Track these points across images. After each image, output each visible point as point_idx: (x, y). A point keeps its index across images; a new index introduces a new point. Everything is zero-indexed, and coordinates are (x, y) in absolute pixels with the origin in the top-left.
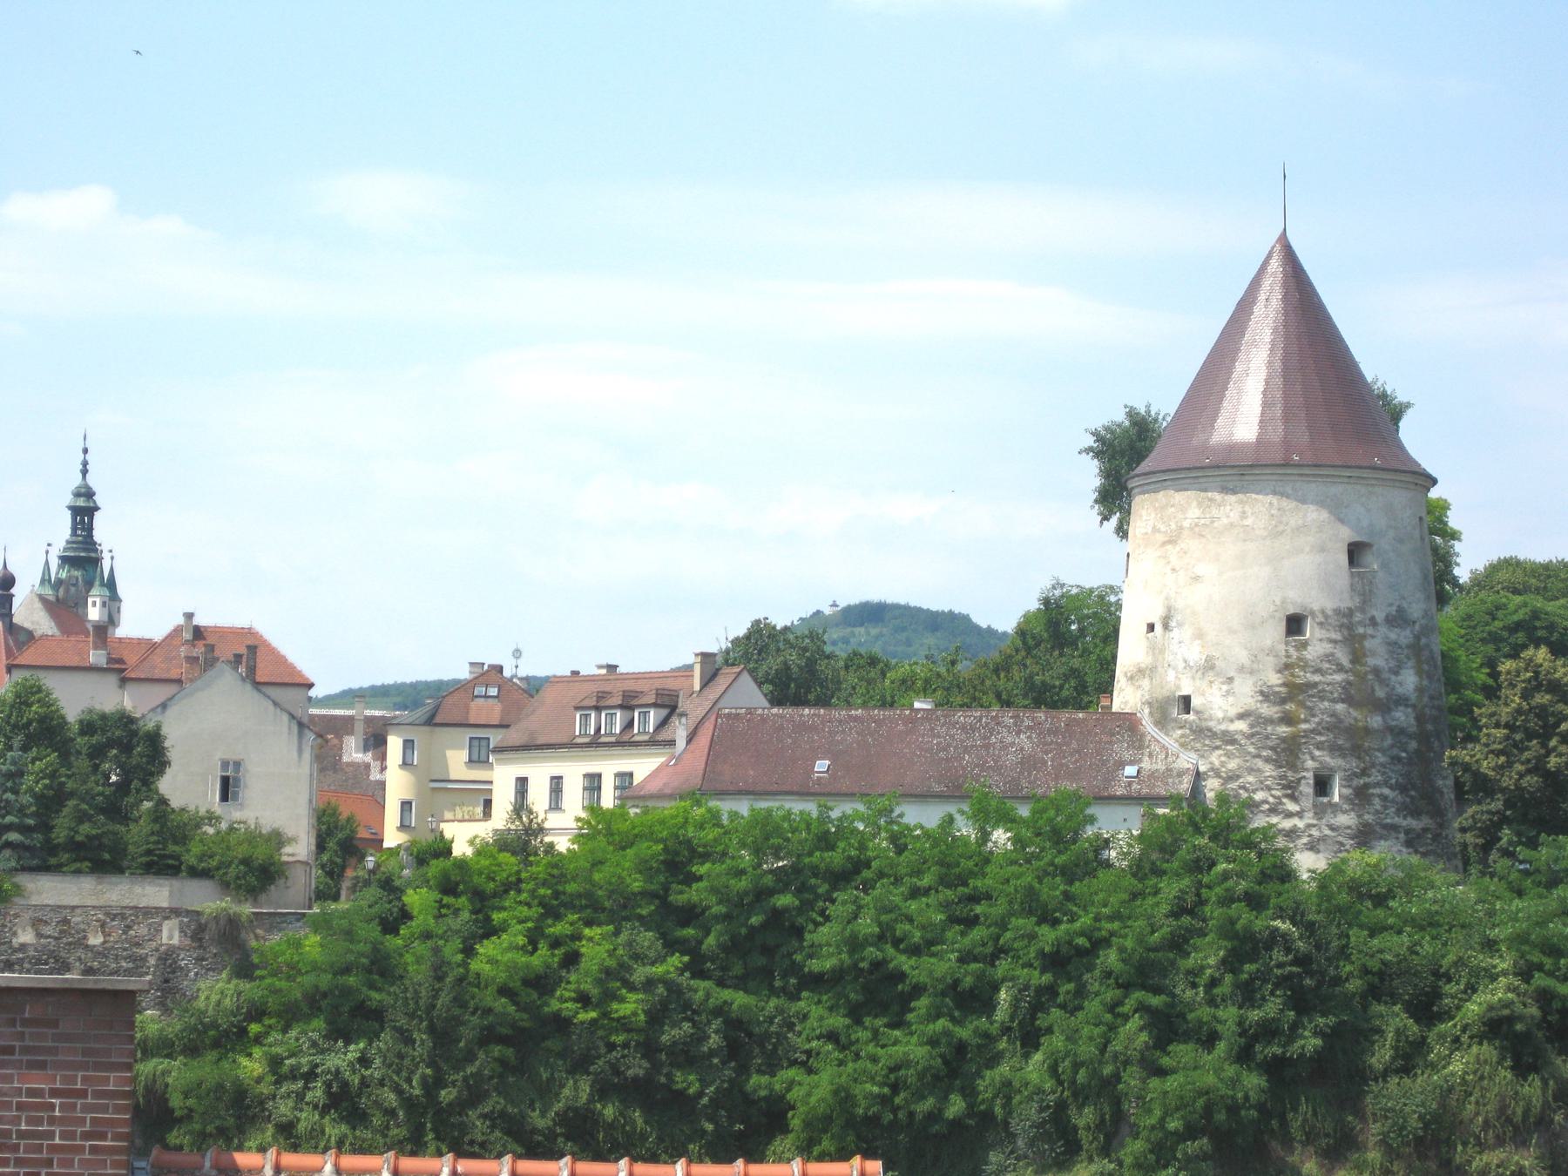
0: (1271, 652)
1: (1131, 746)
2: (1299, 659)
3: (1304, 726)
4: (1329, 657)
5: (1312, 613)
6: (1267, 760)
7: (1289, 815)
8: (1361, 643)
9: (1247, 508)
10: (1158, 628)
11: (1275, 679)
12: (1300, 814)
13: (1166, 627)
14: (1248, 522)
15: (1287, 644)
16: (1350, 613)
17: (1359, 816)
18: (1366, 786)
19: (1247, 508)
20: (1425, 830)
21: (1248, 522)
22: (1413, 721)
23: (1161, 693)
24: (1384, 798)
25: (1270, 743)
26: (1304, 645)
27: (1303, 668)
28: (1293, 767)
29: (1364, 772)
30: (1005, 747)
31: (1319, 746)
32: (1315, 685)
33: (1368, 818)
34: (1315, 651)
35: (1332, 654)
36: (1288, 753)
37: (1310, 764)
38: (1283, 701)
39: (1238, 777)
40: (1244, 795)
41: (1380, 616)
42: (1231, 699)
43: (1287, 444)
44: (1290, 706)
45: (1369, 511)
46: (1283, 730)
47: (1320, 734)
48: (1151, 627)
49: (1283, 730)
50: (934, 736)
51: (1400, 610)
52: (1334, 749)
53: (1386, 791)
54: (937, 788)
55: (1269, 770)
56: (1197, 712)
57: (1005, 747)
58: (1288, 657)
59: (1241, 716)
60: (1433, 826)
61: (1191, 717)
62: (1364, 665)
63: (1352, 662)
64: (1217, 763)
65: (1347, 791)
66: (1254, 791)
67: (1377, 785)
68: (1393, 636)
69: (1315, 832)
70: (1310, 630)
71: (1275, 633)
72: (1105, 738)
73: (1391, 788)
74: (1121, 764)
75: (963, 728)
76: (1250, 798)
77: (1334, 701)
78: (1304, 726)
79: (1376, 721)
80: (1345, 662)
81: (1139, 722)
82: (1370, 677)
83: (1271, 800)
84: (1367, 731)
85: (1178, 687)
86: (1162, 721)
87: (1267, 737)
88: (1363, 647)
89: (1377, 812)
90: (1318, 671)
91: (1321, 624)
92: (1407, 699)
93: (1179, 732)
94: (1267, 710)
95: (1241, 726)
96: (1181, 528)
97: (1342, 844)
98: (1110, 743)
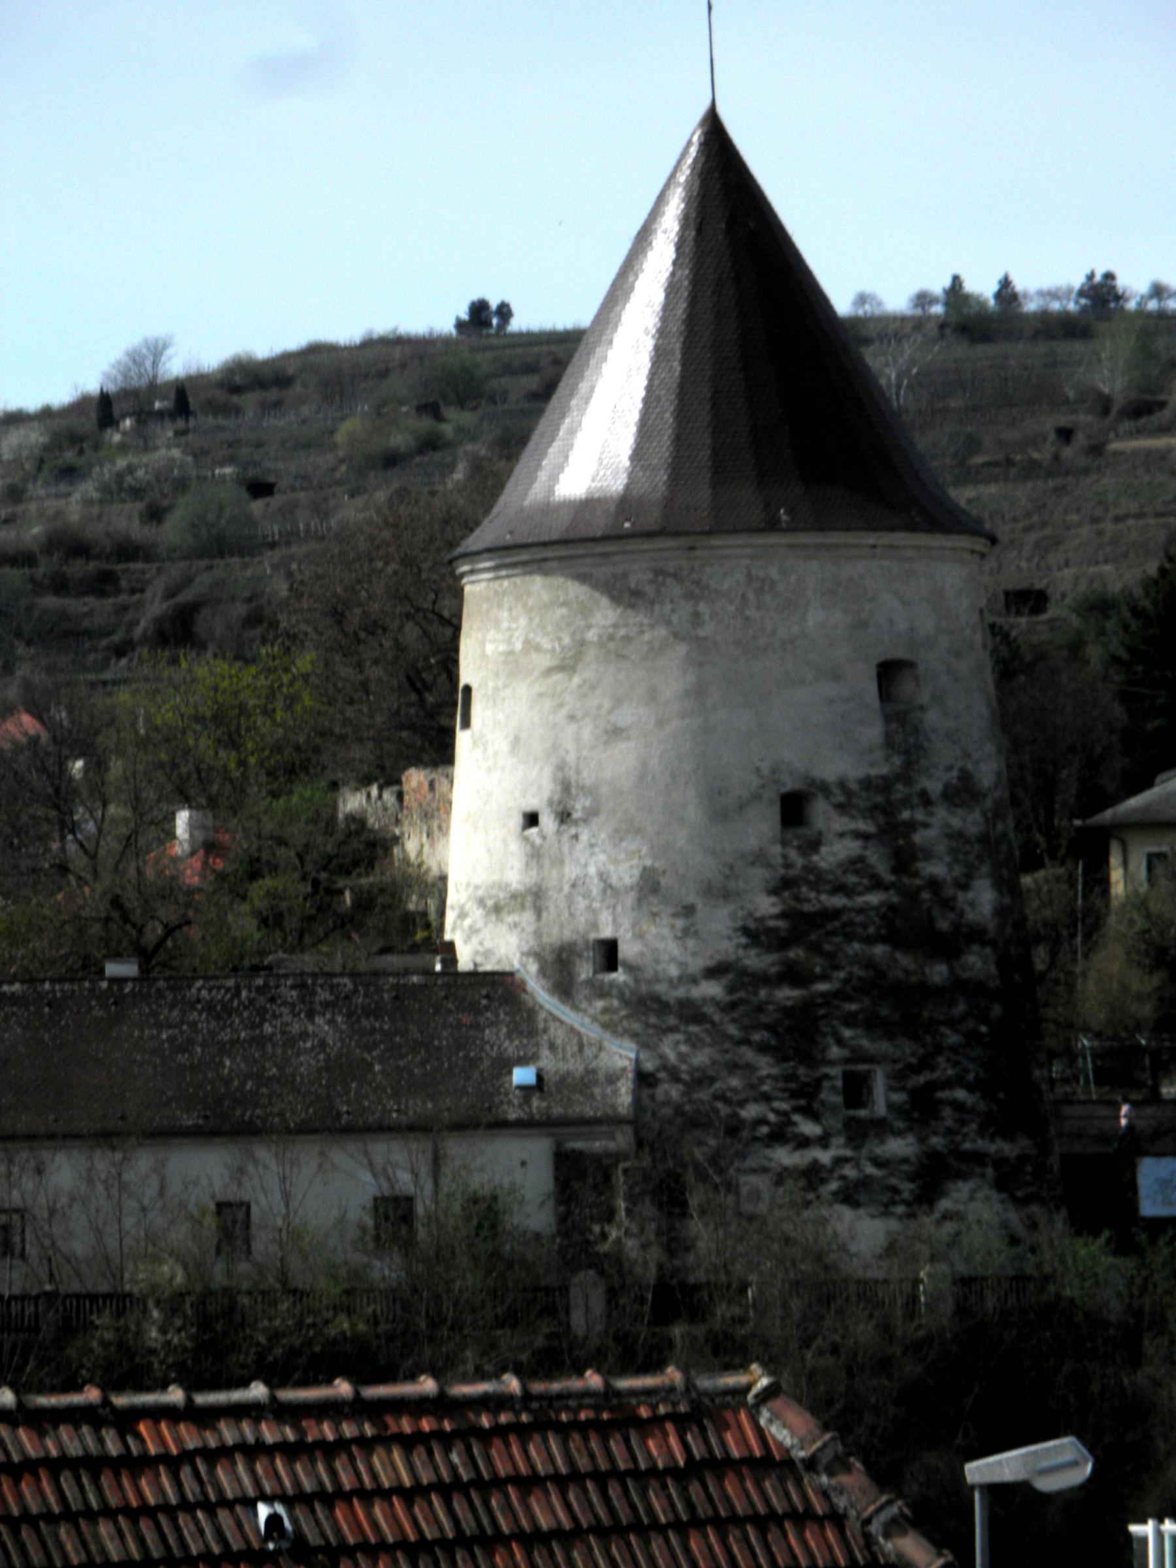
0: (759, 858)
1: (515, 1031)
2: (808, 869)
3: (822, 987)
4: (856, 864)
5: (824, 788)
6: (762, 1048)
7: (804, 1142)
8: (907, 836)
9: (702, 607)
10: (548, 821)
11: (767, 906)
12: (823, 1142)
13: (564, 817)
14: (707, 630)
15: (784, 843)
16: (884, 785)
17: (922, 1140)
18: (932, 1086)
19: (702, 607)
20: (1022, 1159)
21: (707, 630)
22: (993, 970)
23: (555, 935)
24: (958, 1106)
25: (764, 1019)
26: (814, 845)
27: (814, 886)
28: (809, 1060)
29: (925, 1063)
30: (291, 1042)
31: (850, 1020)
32: (836, 913)
33: (936, 1141)
34: (835, 852)
35: (861, 859)
36: (796, 1035)
37: (835, 1052)
38: (784, 944)
39: (712, 1080)
40: (724, 1110)
41: (934, 786)
42: (691, 943)
43: (668, 504)
44: (795, 953)
45: (905, 603)
46: (787, 994)
47: (849, 999)
48: (532, 819)
49: (787, 994)
50: (160, 1026)
51: (965, 777)
52: (871, 1023)
53: (961, 1094)
54: (189, 1121)
55: (765, 1066)
56: (631, 968)
57: (291, 1042)
58: (788, 865)
59: (713, 973)
60: (1033, 1152)
61: (619, 976)
62: (916, 874)
63: (895, 870)
64: (672, 1056)
65: (899, 1097)
66: (742, 1103)
67: (948, 1084)
68: (956, 822)
69: (849, 1171)
70: (822, 816)
71: (760, 828)
72: (467, 1019)
73: (970, 1088)
74: (506, 1065)
75: (210, 1008)
76: (735, 1115)
77: (870, 941)
78: (822, 987)
79: (938, 972)
80: (883, 870)
81: (522, 986)
82: (925, 895)
83: (772, 1117)
84: (926, 991)
85: (595, 926)
86: (564, 988)
87: (760, 1009)
88: (911, 845)
89: (950, 1132)
90: (840, 889)
91: (841, 808)
92: (983, 932)
93: (600, 1004)
94: (754, 960)
95: (712, 989)
96: (582, 643)
97: (895, 1190)
98: (477, 1027)
